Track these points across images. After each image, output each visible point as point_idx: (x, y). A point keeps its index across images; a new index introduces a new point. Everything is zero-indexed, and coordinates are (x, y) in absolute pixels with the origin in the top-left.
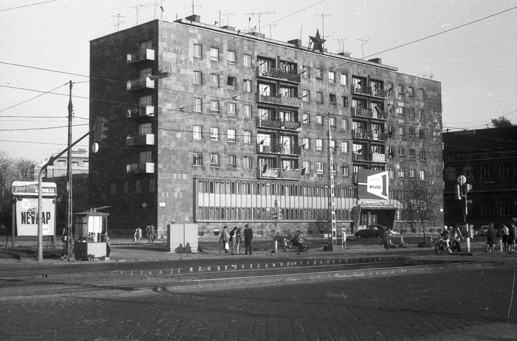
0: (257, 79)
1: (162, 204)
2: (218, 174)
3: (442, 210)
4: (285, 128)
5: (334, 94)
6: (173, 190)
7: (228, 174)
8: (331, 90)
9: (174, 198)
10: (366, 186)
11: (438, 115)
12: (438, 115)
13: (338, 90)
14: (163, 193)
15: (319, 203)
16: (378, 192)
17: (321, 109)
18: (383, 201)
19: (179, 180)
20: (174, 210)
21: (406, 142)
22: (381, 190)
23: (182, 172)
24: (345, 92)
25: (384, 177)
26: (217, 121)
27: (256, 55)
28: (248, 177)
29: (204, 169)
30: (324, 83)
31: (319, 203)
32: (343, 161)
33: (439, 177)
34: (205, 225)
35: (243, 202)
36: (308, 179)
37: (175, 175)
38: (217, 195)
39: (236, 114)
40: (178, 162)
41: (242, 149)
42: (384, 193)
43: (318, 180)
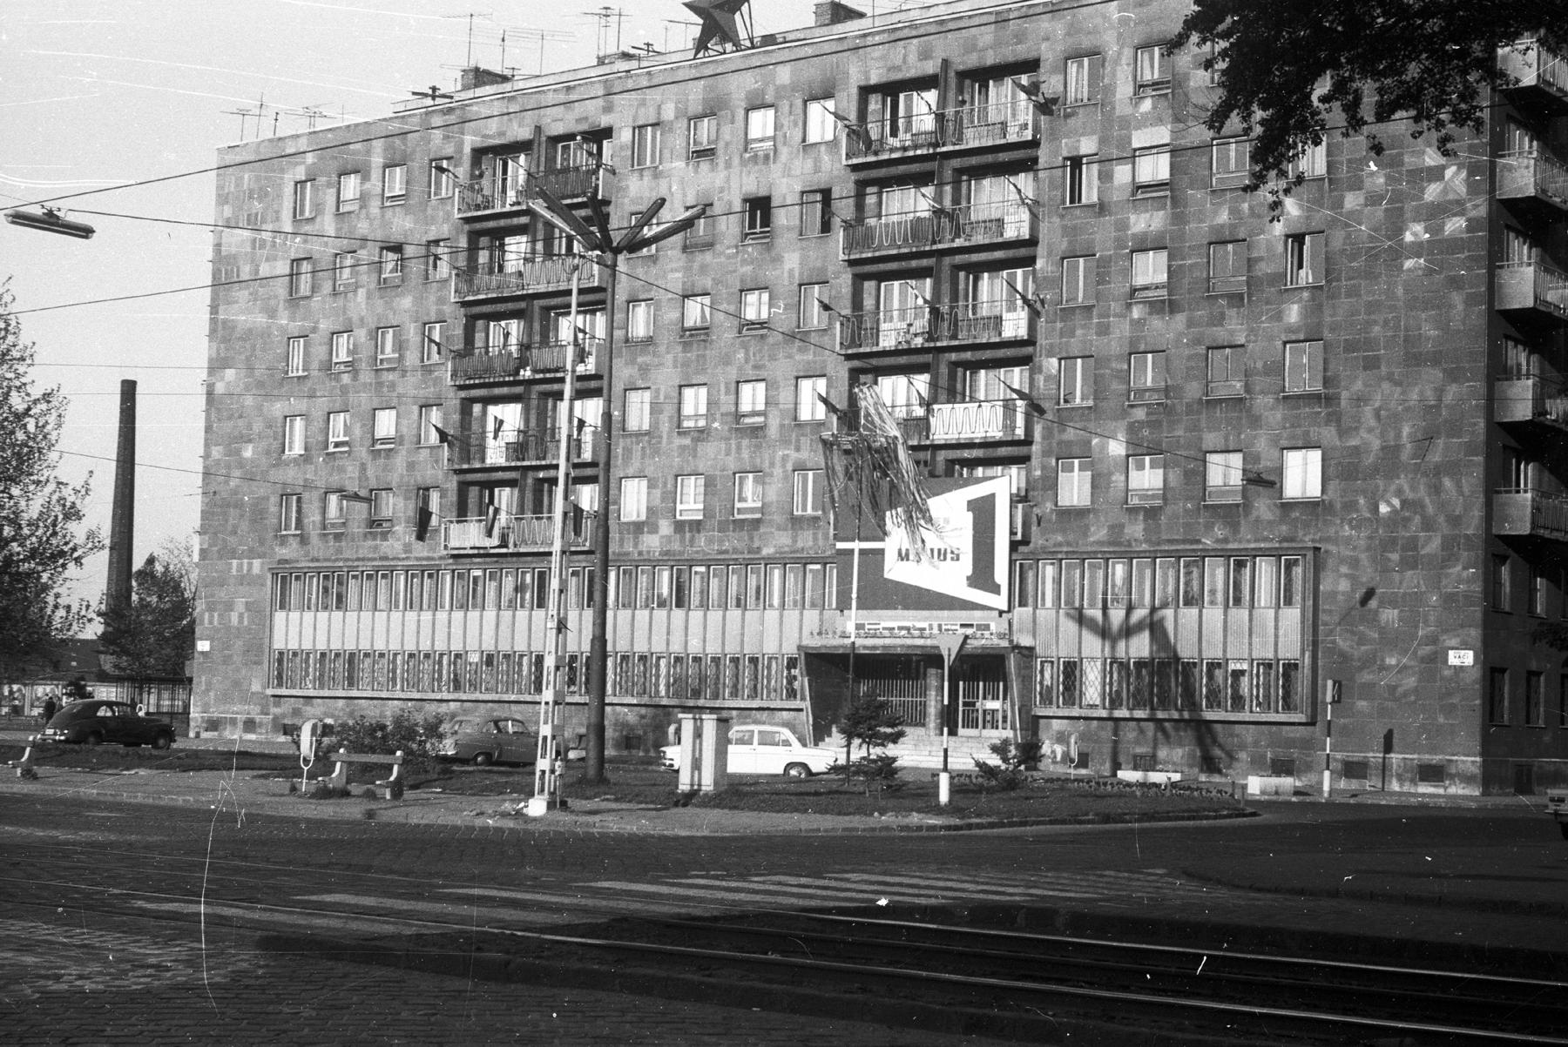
0: (467, 227)
1: (203, 646)
2: (339, 551)
3: (1461, 658)
4: (535, 371)
5: (763, 193)
6: (229, 607)
7: (366, 548)
8: (751, 184)
9: (228, 628)
10: (881, 552)
11: (234, 442)
12: (234, 442)
13: (787, 172)
14: (207, 615)
15: (457, 630)
16: (952, 579)
17: (704, 269)
18: (976, 617)
19: (243, 577)
20: (227, 660)
21: (1180, 319)
22: (966, 566)
23: (252, 554)
24: (817, 170)
25: (983, 511)
26: (344, 390)
27: (467, 150)
28: (425, 554)
29: (303, 540)
30: (722, 165)
31: (457, 630)
32: (794, 455)
33: (1451, 468)
34: (299, 703)
35: (369, 633)
36: (636, 545)
37: (235, 562)
38: (352, 616)
39: (401, 358)
40: (244, 526)
41: (411, 466)
42: (982, 576)
43: (676, 546)
